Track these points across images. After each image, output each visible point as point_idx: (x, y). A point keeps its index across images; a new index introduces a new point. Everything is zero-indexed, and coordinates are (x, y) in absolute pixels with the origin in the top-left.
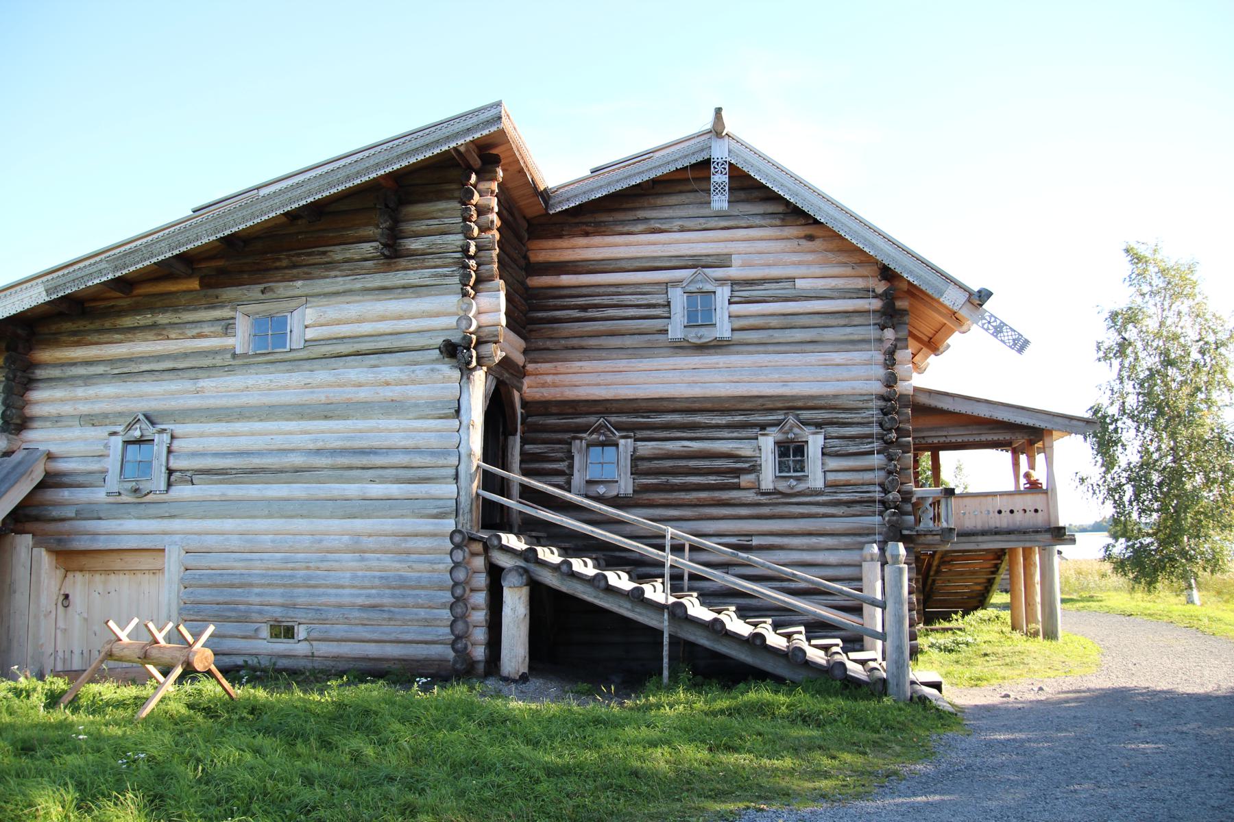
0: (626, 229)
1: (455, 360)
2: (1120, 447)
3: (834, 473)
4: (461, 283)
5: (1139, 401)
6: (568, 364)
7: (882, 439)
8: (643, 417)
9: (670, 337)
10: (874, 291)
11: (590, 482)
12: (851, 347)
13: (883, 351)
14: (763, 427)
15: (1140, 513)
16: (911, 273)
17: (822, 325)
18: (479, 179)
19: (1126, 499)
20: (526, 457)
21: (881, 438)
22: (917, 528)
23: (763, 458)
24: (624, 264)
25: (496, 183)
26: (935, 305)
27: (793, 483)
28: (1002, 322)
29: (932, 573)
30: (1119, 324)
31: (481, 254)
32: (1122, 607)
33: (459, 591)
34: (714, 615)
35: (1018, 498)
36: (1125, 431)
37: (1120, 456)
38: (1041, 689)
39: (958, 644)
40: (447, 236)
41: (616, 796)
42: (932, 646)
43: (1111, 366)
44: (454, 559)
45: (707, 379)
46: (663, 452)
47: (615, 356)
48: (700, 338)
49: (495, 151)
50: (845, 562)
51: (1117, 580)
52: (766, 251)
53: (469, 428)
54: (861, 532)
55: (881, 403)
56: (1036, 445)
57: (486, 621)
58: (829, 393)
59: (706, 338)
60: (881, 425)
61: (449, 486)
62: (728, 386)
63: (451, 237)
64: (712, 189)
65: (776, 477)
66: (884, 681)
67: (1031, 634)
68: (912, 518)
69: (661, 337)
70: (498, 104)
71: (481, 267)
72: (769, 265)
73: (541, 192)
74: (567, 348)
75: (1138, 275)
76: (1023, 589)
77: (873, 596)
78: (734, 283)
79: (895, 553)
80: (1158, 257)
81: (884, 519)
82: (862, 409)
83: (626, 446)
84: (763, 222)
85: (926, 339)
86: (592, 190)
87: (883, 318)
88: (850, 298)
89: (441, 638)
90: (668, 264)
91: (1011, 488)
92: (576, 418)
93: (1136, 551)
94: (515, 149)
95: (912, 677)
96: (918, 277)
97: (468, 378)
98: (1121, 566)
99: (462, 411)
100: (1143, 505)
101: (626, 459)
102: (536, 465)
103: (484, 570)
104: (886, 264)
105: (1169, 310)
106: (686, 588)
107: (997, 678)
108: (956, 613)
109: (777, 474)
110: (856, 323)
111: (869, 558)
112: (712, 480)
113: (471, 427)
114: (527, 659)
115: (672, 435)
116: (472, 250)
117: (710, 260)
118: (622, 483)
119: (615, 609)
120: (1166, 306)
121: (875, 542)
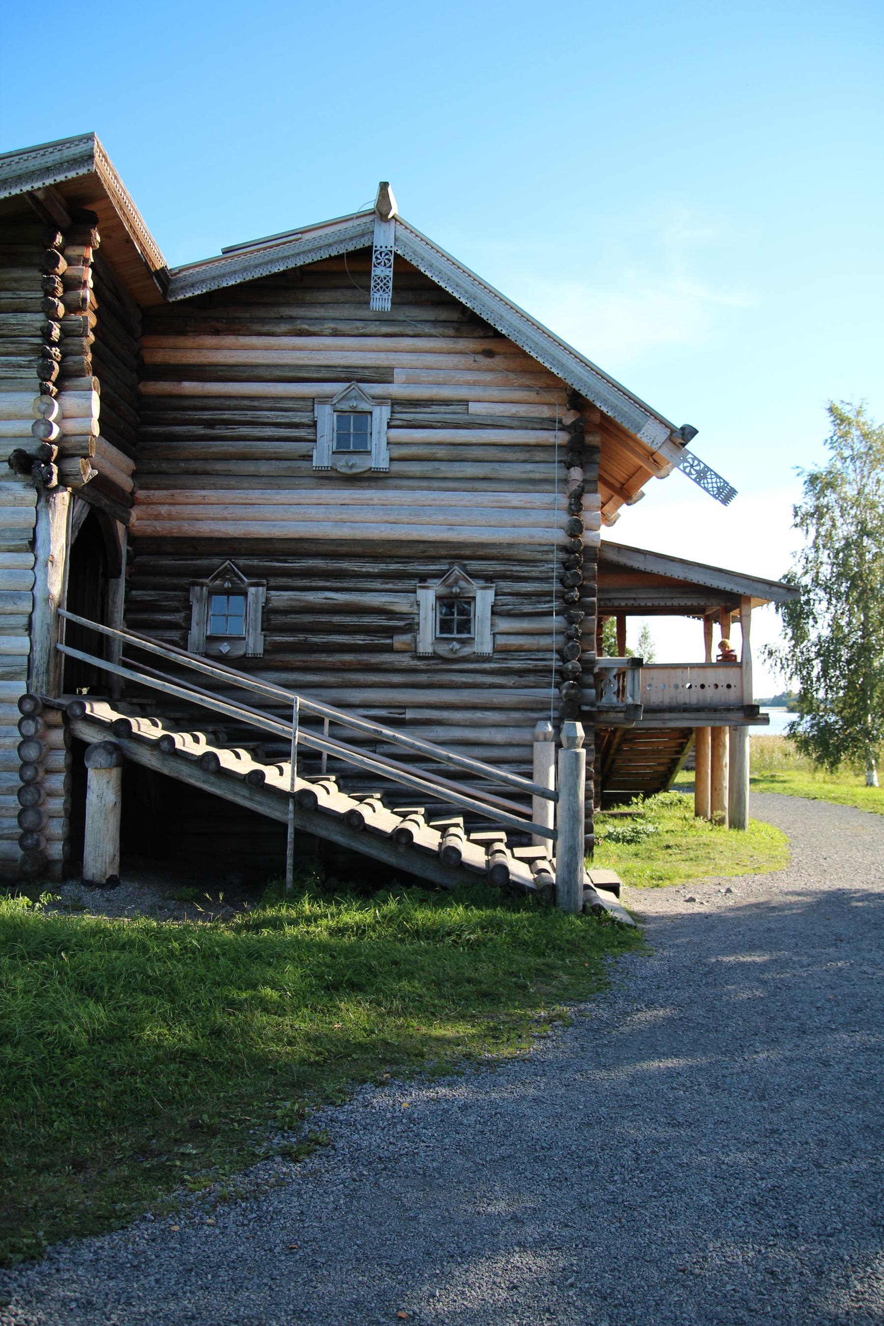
0: (266, 328)
1: (30, 477)
2: (811, 622)
3: (505, 637)
4: (40, 377)
5: (832, 572)
6: (188, 493)
7: (563, 597)
8: (279, 561)
9: (314, 464)
10: (560, 422)
11: (211, 639)
12: (530, 487)
13: (568, 494)
14: (423, 578)
15: (826, 691)
16: (605, 401)
17: (497, 459)
18: (68, 242)
19: (814, 674)
20: (131, 605)
21: (561, 596)
22: (599, 704)
23: (422, 612)
24: (262, 372)
25: (91, 250)
26: (631, 443)
27: (457, 646)
28: (706, 466)
29: (612, 752)
30: (818, 488)
31: (69, 341)
32: (806, 789)
33: (29, 773)
34: (352, 804)
35: (710, 672)
36: (817, 602)
37: (811, 629)
38: (729, 891)
39: (637, 832)
40: (24, 314)
41: (183, 1070)
42: (609, 836)
43: (807, 532)
44: (24, 731)
45: (358, 517)
46: (302, 604)
47: (246, 485)
48: (351, 467)
49: (91, 208)
50: (514, 742)
51: (800, 759)
52: (435, 366)
53: (47, 565)
54: (535, 706)
55: (563, 555)
56: (732, 614)
57: (66, 810)
58: (502, 541)
59: (359, 468)
60: (562, 581)
61: (20, 638)
62: (383, 527)
63: (29, 317)
64: (373, 284)
65: (436, 638)
66: (553, 888)
67: (716, 821)
68: (593, 691)
69: (303, 464)
70: (90, 138)
71: (69, 358)
72: (438, 384)
73: (157, 271)
74: (187, 473)
75: (840, 437)
76: (709, 771)
77: (541, 786)
78: (396, 403)
79: (571, 735)
80: (862, 419)
81: (561, 692)
82: (540, 561)
83: (256, 595)
84: (433, 331)
85: (618, 485)
86: (224, 276)
87: (570, 454)
88: (533, 429)
89: (6, 831)
90: (316, 375)
91: (702, 660)
92: (197, 559)
93: (820, 730)
94: (114, 203)
95: (587, 881)
96: (613, 408)
97: (48, 501)
98: (804, 745)
99: (39, 544)
100: (830, 681)
101: (256, 611)
102: (146, 616)
103: (64, 746)
104: (577, 389)
105: (868, 477)
106: (324, 768)
107: (680, 877)
108: (636, 796)
109: (438, 635)
110: (538, 459)
111: (541, 737)
112: (359, 640)
113: (50, 564)
114: (118, 858)
115: (314, 584)
116: (56, 333)
117: (367, 373)
118: (251, 641)
119: (230, 796)
120: (866, 473)
121: (549, 719)
